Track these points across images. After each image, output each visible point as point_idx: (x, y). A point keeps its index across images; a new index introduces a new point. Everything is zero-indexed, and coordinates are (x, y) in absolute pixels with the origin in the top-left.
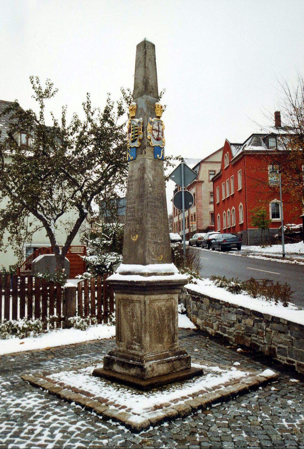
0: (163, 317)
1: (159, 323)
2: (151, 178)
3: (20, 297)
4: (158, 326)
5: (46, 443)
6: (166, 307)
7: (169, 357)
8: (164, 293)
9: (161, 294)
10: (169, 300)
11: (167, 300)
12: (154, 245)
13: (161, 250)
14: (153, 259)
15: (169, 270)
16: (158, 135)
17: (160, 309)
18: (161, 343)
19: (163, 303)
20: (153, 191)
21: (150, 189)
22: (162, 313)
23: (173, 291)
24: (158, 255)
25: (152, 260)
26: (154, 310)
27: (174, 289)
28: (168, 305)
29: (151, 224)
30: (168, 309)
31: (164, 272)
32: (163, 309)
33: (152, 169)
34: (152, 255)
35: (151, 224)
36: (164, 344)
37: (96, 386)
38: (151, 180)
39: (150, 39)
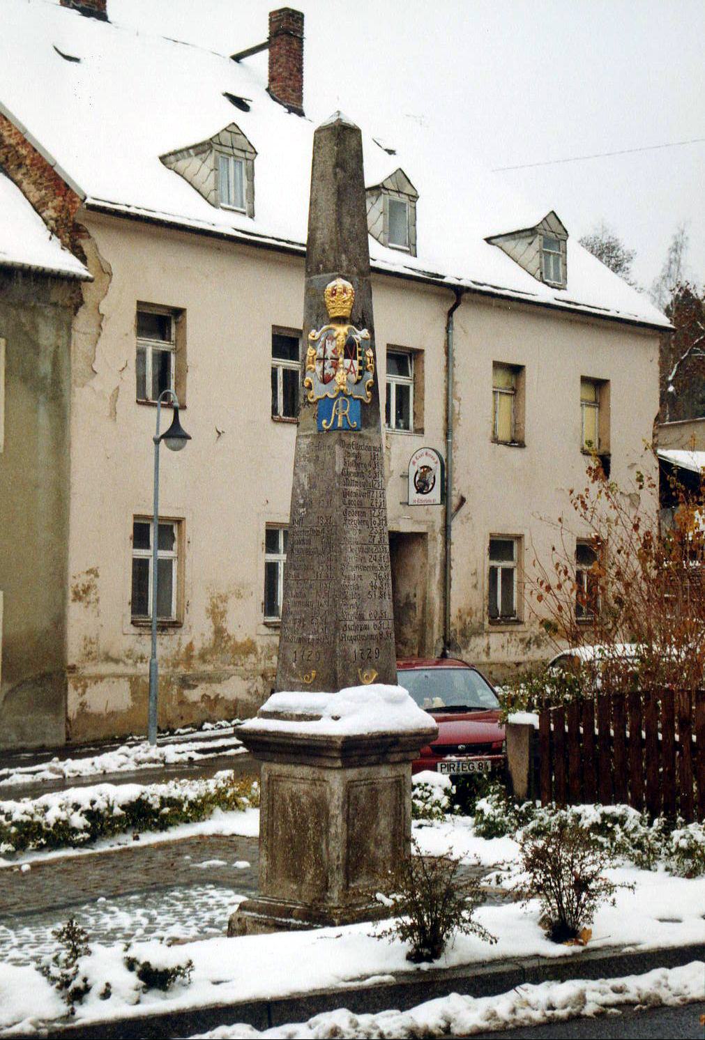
0: (305, 821)
1: (294, 832)
2: (306, 483)
3: (581, 735)
4: (291, 840)
5: (40, 954)
6: (311, 797)
7: (291, 917)
8: (302, 764)
9: (296, 764)
10: (318, 783)
11: (314, 782)
12: (297, 645)
13: (313, 657)
14: (293, 680)
15: (312, 708)
16: (324, 368)
17: (295, 798)
18: (296, 882)
19: (304, 787)
20: (308, 514)
21: (301, 510)
22: (302, 810)
23: (318, 761)
24: (306, 670)
25: (291, 683)
26: (284, 800)
27: (320, 756)
28: (315, 794)
29: (296, 596)
30: (317, 805)
31: (299, 712)
32: (302, 800)
33: (309, 461)
34: (291, 670)
35: (296, 596)
36: (304, 887)
37: (543, 1002)
38: (306, 487)
39: (351, 119)
